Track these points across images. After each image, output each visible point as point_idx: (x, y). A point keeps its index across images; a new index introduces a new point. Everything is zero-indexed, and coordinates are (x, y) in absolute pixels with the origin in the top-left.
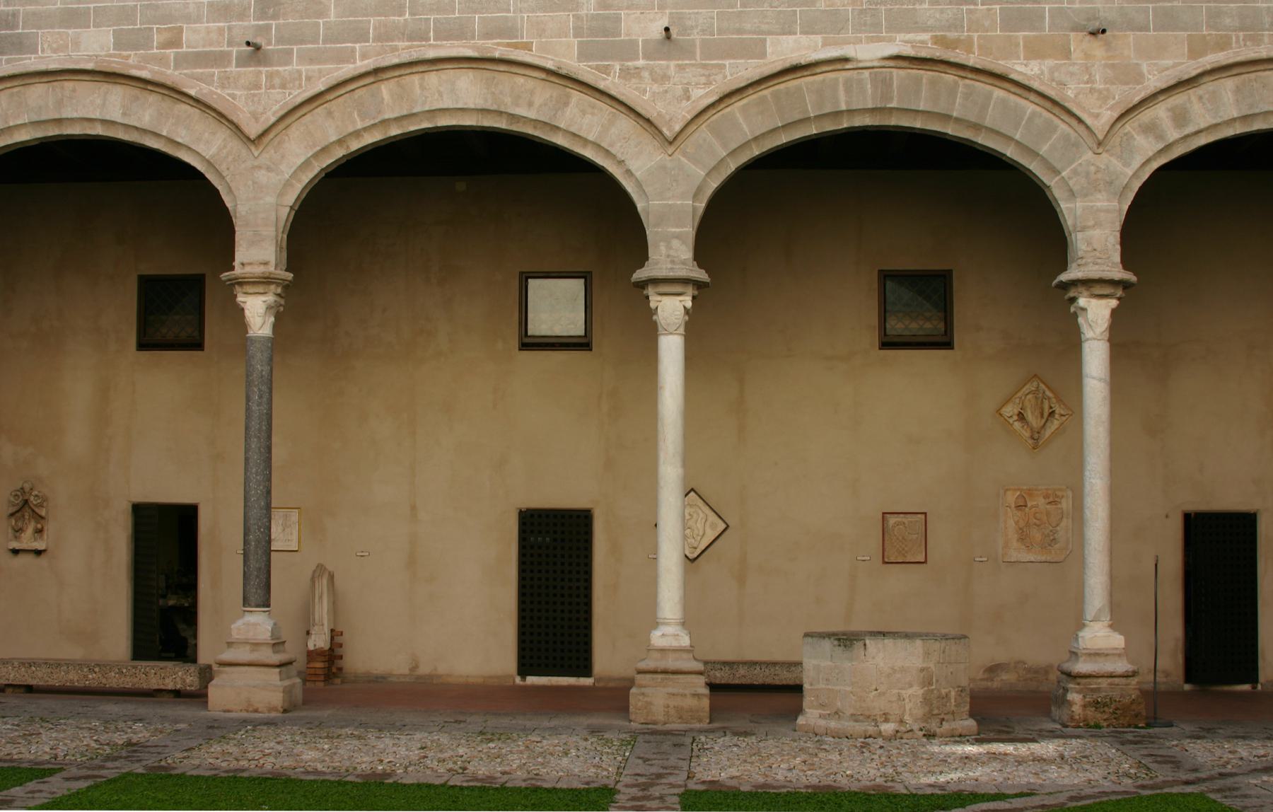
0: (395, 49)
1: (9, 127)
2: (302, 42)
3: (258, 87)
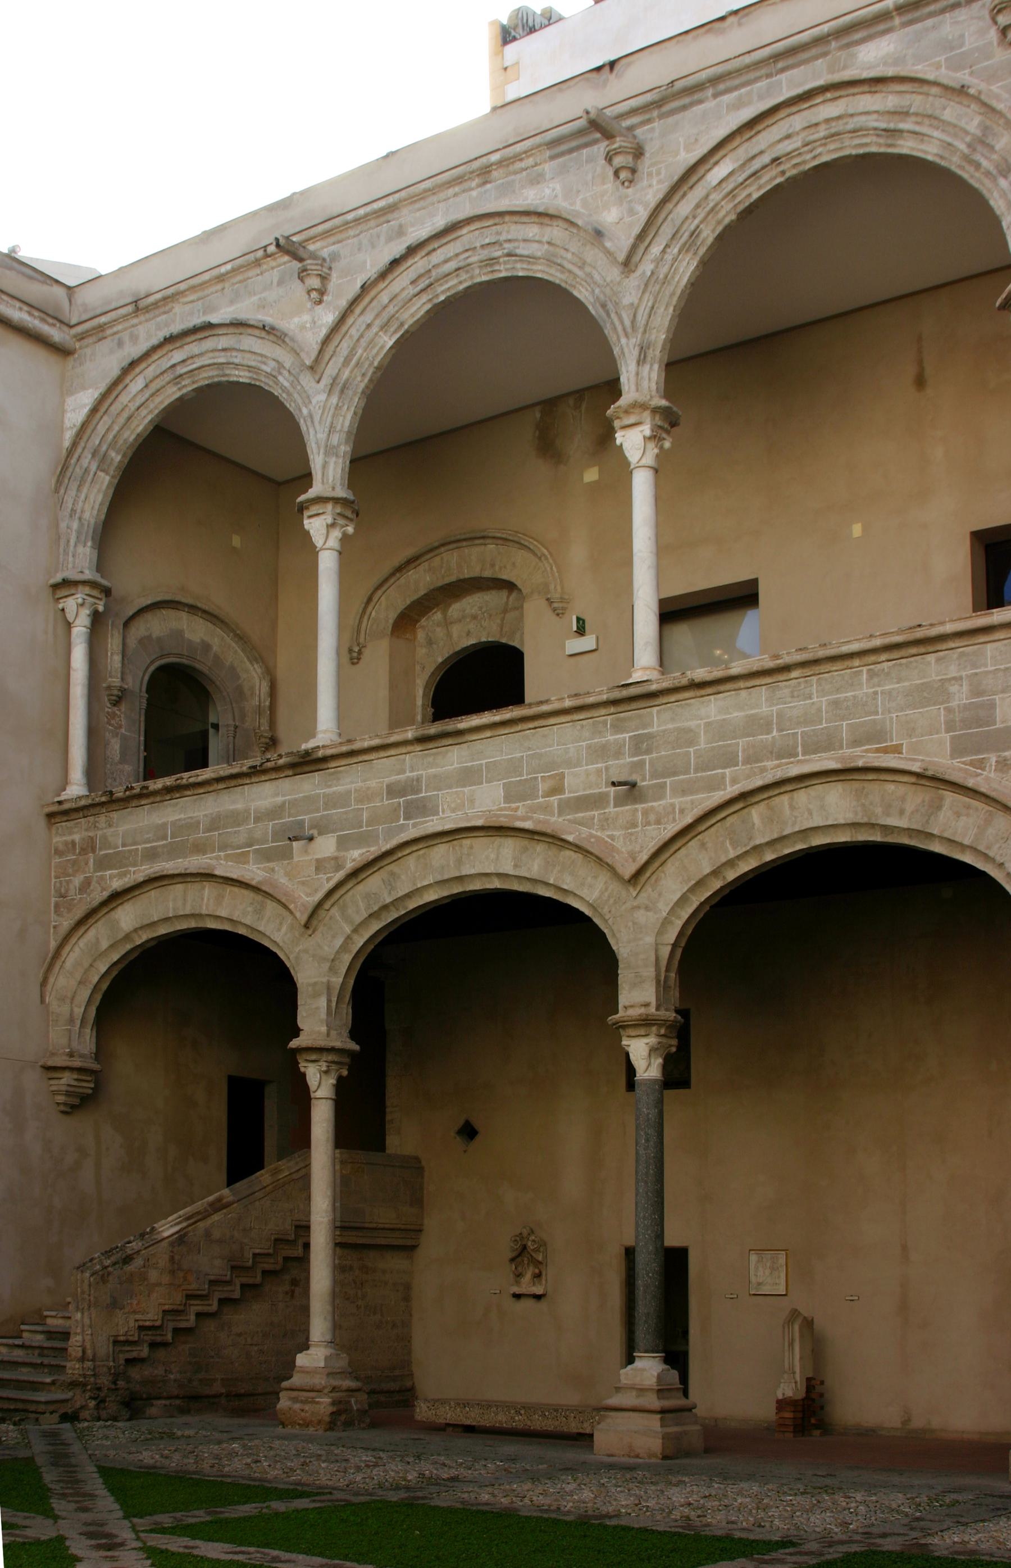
0: (763, 770)
1: (418, 889)
2: (675, 774)
3: (634, 825)
